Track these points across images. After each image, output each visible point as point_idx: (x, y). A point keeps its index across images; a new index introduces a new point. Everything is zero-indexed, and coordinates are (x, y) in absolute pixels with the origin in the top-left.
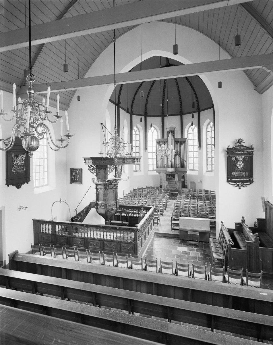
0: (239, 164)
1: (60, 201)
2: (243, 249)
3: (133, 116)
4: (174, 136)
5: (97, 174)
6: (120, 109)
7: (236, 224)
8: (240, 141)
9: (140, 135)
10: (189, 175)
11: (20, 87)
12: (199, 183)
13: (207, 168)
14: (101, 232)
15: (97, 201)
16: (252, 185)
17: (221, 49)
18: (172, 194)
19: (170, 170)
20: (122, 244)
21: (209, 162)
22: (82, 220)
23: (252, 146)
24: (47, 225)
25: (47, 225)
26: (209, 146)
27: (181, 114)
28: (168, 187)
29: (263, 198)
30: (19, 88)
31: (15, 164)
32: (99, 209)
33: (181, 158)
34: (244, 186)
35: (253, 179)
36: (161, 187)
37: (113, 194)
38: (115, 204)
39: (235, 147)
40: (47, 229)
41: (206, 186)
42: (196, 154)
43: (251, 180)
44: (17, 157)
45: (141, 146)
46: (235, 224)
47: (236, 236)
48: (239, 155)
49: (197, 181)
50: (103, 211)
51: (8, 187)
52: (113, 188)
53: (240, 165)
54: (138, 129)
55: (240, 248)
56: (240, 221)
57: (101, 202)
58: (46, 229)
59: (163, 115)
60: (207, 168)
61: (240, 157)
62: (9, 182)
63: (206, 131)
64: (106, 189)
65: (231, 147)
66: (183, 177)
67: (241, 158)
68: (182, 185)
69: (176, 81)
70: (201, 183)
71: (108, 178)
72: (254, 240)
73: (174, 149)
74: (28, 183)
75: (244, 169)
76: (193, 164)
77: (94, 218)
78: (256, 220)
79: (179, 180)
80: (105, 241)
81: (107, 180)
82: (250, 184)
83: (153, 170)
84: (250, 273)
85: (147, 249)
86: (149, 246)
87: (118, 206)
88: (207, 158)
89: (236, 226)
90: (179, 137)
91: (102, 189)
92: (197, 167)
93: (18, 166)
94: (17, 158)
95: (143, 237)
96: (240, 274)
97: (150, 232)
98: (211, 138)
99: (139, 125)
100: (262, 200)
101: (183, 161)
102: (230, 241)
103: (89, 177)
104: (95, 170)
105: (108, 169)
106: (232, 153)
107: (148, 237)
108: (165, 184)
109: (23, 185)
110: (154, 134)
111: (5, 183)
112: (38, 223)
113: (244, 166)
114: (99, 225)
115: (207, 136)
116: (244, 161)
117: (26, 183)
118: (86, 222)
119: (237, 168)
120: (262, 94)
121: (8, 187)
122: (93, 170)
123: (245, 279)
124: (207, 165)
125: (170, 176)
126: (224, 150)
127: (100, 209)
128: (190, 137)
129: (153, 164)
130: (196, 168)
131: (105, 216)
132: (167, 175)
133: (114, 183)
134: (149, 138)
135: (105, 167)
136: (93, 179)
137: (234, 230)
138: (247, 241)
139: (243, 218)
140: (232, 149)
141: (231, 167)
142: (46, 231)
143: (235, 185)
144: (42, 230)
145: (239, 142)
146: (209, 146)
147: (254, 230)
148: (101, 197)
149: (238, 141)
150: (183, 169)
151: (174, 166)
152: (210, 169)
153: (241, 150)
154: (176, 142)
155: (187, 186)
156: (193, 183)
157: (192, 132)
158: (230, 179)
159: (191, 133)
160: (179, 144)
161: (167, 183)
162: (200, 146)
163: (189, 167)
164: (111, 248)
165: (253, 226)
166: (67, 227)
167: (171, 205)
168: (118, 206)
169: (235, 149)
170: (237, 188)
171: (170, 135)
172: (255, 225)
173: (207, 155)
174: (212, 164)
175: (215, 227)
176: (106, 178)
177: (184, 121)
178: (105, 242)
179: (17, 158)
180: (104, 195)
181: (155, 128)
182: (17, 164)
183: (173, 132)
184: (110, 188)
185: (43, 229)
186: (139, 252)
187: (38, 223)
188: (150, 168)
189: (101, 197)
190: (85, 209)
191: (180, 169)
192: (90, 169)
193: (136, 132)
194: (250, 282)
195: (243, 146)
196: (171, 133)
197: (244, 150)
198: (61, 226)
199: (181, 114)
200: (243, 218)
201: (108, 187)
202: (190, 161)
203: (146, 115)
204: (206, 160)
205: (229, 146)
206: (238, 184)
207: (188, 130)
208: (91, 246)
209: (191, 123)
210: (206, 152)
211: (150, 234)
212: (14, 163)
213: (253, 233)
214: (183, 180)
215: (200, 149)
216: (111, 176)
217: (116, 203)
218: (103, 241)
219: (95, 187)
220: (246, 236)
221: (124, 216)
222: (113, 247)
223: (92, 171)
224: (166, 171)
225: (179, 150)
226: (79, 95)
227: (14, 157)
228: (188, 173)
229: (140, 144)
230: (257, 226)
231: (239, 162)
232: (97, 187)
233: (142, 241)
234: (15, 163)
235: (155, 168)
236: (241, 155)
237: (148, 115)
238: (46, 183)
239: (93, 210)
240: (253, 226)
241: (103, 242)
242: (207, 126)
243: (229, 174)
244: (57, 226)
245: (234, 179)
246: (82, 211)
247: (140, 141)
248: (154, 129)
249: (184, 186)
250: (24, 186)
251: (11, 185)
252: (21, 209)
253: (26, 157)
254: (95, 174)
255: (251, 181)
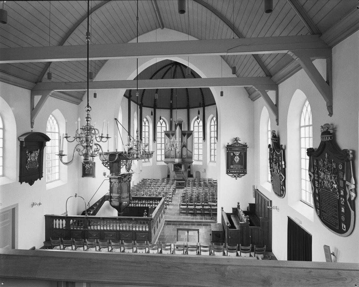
0: (236, 158)
1: (76, 196)
2: (237, 229)
3: (144, 108)
4: (181, 128)
5: (110, 167)
6: (132, 102)
7: (233, 209)
8: (237, 139)
9: (149, 126)
10: (195, 165)
11: (36, 83)
12: (203, 172)
13: (211, 159)
14: (114, 223)
15: (110, 194)
16: (246, 175)
17: (223, 60)
18: (179, 183)
19: (177, 161)
20: (137, 233)
21: (213, 153)
22: (94, 214)
23: (246, 143)
24: (61, 220)
25: (61, 220)
26: (213, 139)
27: (188, 107)
28: (176, 176)
29: (254, 187)
30: (35, 84)
31: (29, 161)
32: (113, 201)
33: (187, 150)
34: (239, 177)
35: (246, 171)
36: (169, 176)
37: (127, 187)
38: (128, 197)
39: (233, 144)
40: (60, 224)
41: (209, 175)
42: (201, 146)
43: (245, 172)
44: (31, 153)
45: (150, 137)
46: (232, 209)
47: (233, 219)
48: (236, 151)
49: (201, 171)
50: (116, 204)
51: (21, 184)
52: (127, 181)
53: (237, 159)
54: (147, 120)
55: (235, 228)
56: (236, 207)
57: (115, 195)
58: (59, 224)
59: (171, 108)
60: (211, 159)
61: (237, 153)
62: (22, 179)
63: (210, 125)
64: (120, 182)
65: (230, 144)
66: (189, 167)
67: (237, 153)
68: (188, 175)
69: (187, 90)
70: (206, 173)
71: (121, 172)
72: (245, 221)
73: (182, 142)
74: (40, 179)
75: (240, 163)
76: (199, 155)
77: (109, 211)
78: (249, 205)
79: (186, 170)
80: (120, 232)
81: (121, 174)
82: (245, 175)
83: (162, 161)
84: (243, 247)
85: (159, 236)
86: (161, 233)
87: (131, 198)
88: (211, 149)
89: (233, 211)
90: (186, 129)
91: (116, 183)
92: (202, 157)
93: (31, 162)
94: (31, 154)
95: (156, 225)
96: (236, 249)
97: (162, 220)
98: (215, 131)
99: (148, 117)
100: (253, 188)
101: (190, 153)
102: (228, 224)
103: (101, 170)
104: (109, 163)
105: (122, 163)
106: (231, 149)
107: (159, 225)
108: (173, 174)
109: (35, 182)
110: (163, 127)
111: (19, 180)
112: (50, 219)
113: (240, 160)
114: (115, 217)
115: (210, 129)
116: (240, 156)
117: (38, 179)
118: (100, 214)
119: (235, 161)
120: (254, 101)
121: (21, 184)
122: (107, 164)
123: (239, 252)
124: (211, 155)
125: (177, 167)
126: (224, 146)
127: (114, 202)
128: (196, 129)
129: (161, 155)
130: (201, 158)
131: (118, 208)
132: (175, 165)
133: (128, 176)
134: (158, 129)
135: (118, 162)
136: (104, 173)
137: (232, 214)
138: (240, 223)
139: (239, 203)
140: (231, 146)
141: (230, 161)
142: (59, 226)
143: (232, 176)
144: (55, 225)
145: (236, 140)
146: (213, 139)
147: (245, 213)
148: (115, 189)
149: (236, 139)
150: (189, 160)
151: (181, 157)
152: (213, 159)
153: (237, 147)
154: (183, 134)
155: (192, 175)
156: (198, 173)
157: (197, 125)
158: (229, 171)
159: (196, 126)
160: (186, 136)
161: (174, 173)
162: (204, 138)
163: (195, 157)
164: (126, 237)
165: (246, 210)
166: (78, 220)
167: (178, 194)
168: (131, 198)
169: (233, 146)
170: (234, 178)
171: (178, 128)
172: (248, 209)
173: (211, 147)
174: (215, 155)
175: (217, 214)
176: (119, 171)
177: (191, 114)
178: (120, 233)
179: (31, 154)
180: (118, 188)
181: (164, 121)
182: (31, 160)
183: (180, 125)
184: (124, 181)
185: (56, 224)
186: (153, 239)
187: (50, 219)
188: (159, 158)
189: (115, 189)
190: (98, 202)
191: (187, 160)
192: (103, 163)
193: (145, 124)
194: (242, 254)
195: (239, 143)
196: (179, 126)
197: (240, 147)
198: (73, 221)
199: (188, 107)
200: (239, 203)
201: (123, 180)
202: (196, 152)
203: (155, 107)
204: (209, 151)
205: (228, 144)
206: (235, 175)
207: (194, 123)
208: (107, 237)
209: (197, 117)
210: (209, 126)
211: (161, 222)
212: (28, 160)
213: (246, 215)
214: (189, 170)
215: (204, 141)
216: (123, 171)
217: (130, 195)
218: (119, 232)
219: (109, 181)
220: (240, 219)
221: (143, 207)
222: (128, 237)
223: (106, 164)
224: (173, 162)
225: (186, 142)
226: (96, 93)
227: (28, 153)
228: (194, 163)
229: (149, 135)
230: (249, 209)
231: (236, 157)
232: (111, 181)
233: (155, 230)
234: (29, 159)
235: (163, 158)
236: (238, 151)
237: (157, 107)
238: (57, 178)
239: (107, 203)
240: (246, 210)
241: (119, 233)
242: (211, 120)
243: (228, 167)
244: (54, 220)
245: (232, 171)
246: (95, 204)
247: (149, 132)
248: (163, 121)
249: (190, 176)
250: (37, 182)
251: (24, 182)
252: (34, 206)
253: (39, 153)
254: (109, 167)
255: (245, 173)
